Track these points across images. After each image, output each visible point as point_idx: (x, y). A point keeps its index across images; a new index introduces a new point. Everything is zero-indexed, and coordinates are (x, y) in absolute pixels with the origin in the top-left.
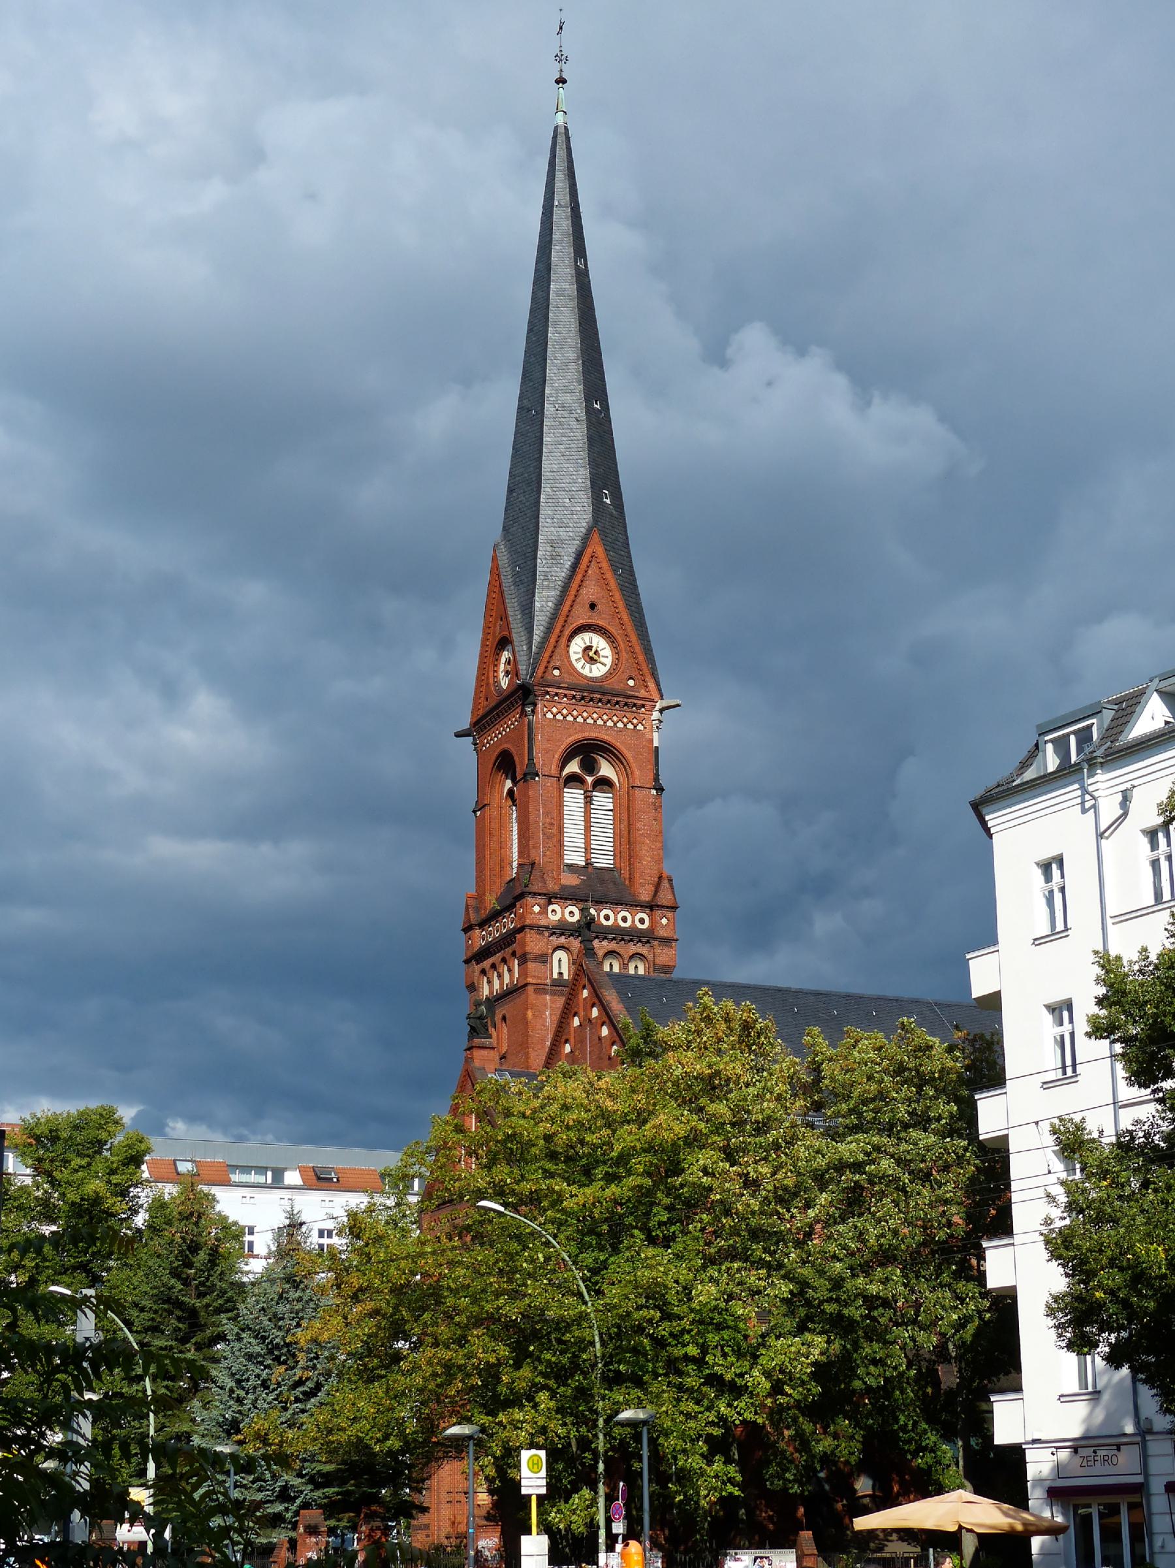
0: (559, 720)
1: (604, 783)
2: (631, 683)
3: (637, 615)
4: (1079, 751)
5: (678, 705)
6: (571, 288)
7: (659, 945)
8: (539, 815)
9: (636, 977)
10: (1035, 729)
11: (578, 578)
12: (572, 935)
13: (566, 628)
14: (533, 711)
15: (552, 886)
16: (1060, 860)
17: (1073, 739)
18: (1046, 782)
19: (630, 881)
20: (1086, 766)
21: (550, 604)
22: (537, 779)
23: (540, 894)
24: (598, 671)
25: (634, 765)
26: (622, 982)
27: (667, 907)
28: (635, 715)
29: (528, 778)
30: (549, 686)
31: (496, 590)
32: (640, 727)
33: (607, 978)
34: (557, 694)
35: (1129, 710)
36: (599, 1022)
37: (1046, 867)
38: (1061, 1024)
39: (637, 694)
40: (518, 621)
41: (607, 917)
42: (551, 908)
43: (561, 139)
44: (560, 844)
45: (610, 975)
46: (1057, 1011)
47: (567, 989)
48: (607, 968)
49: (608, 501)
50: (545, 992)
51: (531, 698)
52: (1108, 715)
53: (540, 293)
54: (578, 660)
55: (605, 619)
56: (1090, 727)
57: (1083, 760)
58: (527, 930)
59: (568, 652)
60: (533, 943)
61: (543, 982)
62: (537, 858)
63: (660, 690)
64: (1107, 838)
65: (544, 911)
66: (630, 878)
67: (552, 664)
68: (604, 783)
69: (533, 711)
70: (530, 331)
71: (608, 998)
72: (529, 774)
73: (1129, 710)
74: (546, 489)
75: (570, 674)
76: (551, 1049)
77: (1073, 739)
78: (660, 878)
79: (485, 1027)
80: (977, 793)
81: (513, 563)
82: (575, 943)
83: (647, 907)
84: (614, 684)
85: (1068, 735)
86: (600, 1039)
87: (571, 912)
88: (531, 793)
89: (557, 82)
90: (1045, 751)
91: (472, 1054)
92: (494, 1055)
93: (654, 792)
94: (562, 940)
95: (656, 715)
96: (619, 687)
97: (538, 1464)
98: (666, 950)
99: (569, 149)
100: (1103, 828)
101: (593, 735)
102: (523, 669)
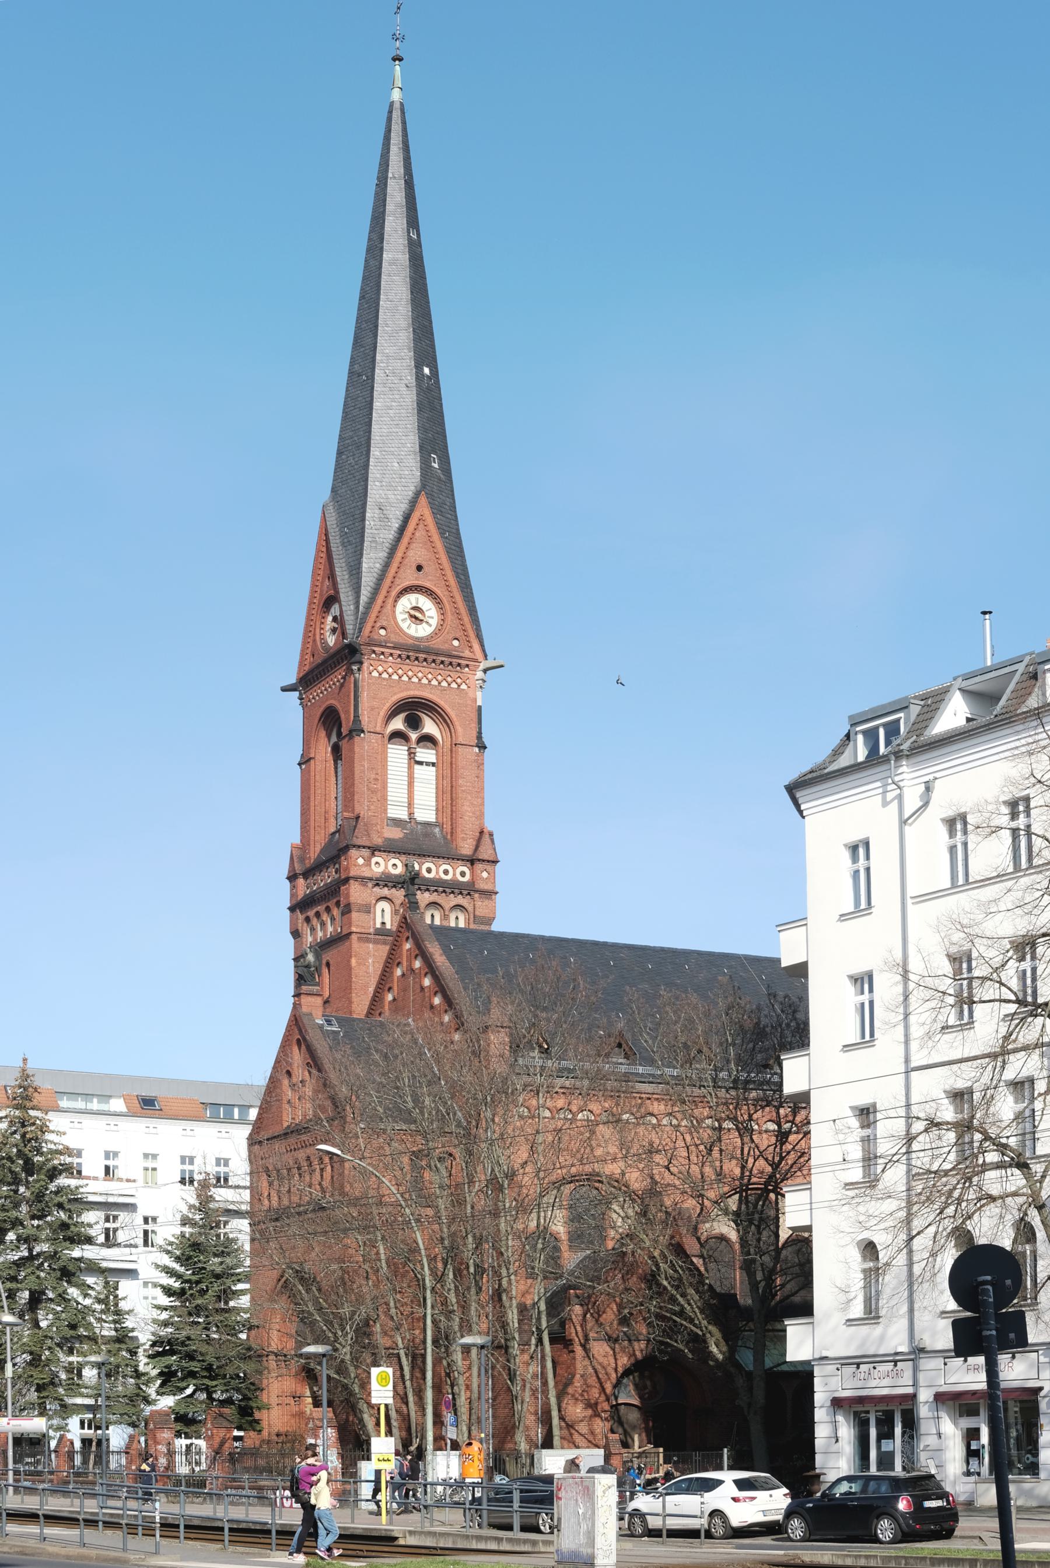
0: (384, 679)
1: (427, 740)
2: (456, 643)
3: (462, 577)
4: (888, 743)
5: (502, 666)
6: (404, 258)
7: (480, 898)
8: (362, 768)
9: (457, 929)
10: (847, 720)
11: (405, 540)
12: (394, 886)
13: (392, 589)
14: (359, 670)
15: (378, 841)
16: (867, 844)
17: (882, 732)
18: (856, 768)
19: (452, 836)
20: (893, 757)
21: (378, 565)
22: (362, 735)
23: (364, 847)
24: (421, 631)
25: (457, 723)
26: (443, 933)
27: (488, 861)
28: (459, 674)
29: (354, 734)
30: (375, 645)
31: (324, 549)
32: (464, 686)
33: (430, 931)
34: (383, 653)
35: (934, 707)
36: (423, 972)
37: (854, 849)
38: (862, 993)
39: (461, 654)
40: (346, 581)
41: (430, 869)
42: (374, 860)
43: (396, 115)
44: (384, 799)
45: (432, 926)
46: (859, 982)
47: (391, 938)
48: (428, 921)
49: (436, 466)
50: (368, 941)
51: (357, 657)
52: (915, 710)
53: (372, 262)
54: (404, 620)
55: (432, 581)
56: (898, 720)
57: (890, 753)
58: (352, 882)
59: (394, 612)
60: (356, 893)
61: (367, 931)
62: (362, 813)
63: (484, 651)
64: (910, 825)
65: (368, 862)
66: (452, 833)
67: (378, 624)
68: (427, 740)
69: (359, 670)
70: (362, 297)
71: (431, 950)
72: (355, 730)
73: (934, 707)
74: (375, 452)
75: (396, 634)
76: (374, 996)
77: (882, 732)
78: (482, 833)
79: (312, 975)
80: (792, 776)
81: (341, 525)
82: (399, 895)
83: (468, 861)
84: (437, 644)
85: (877, 728)
86: (422, 989)
87: (394, 865)
88: (357, 749)
89: (394, 59)
90: (855, 741)
91: (300, 1000)
92: (319, 1001)
93: (477, 750)
94: (385, 892)
95: (480, 674)
96: (444, 647)
97: (386, 1379)
98: (486, 902)
99: (404, 123)
100: (906, 815)
101: (417, 693)
102: (349, 628)
